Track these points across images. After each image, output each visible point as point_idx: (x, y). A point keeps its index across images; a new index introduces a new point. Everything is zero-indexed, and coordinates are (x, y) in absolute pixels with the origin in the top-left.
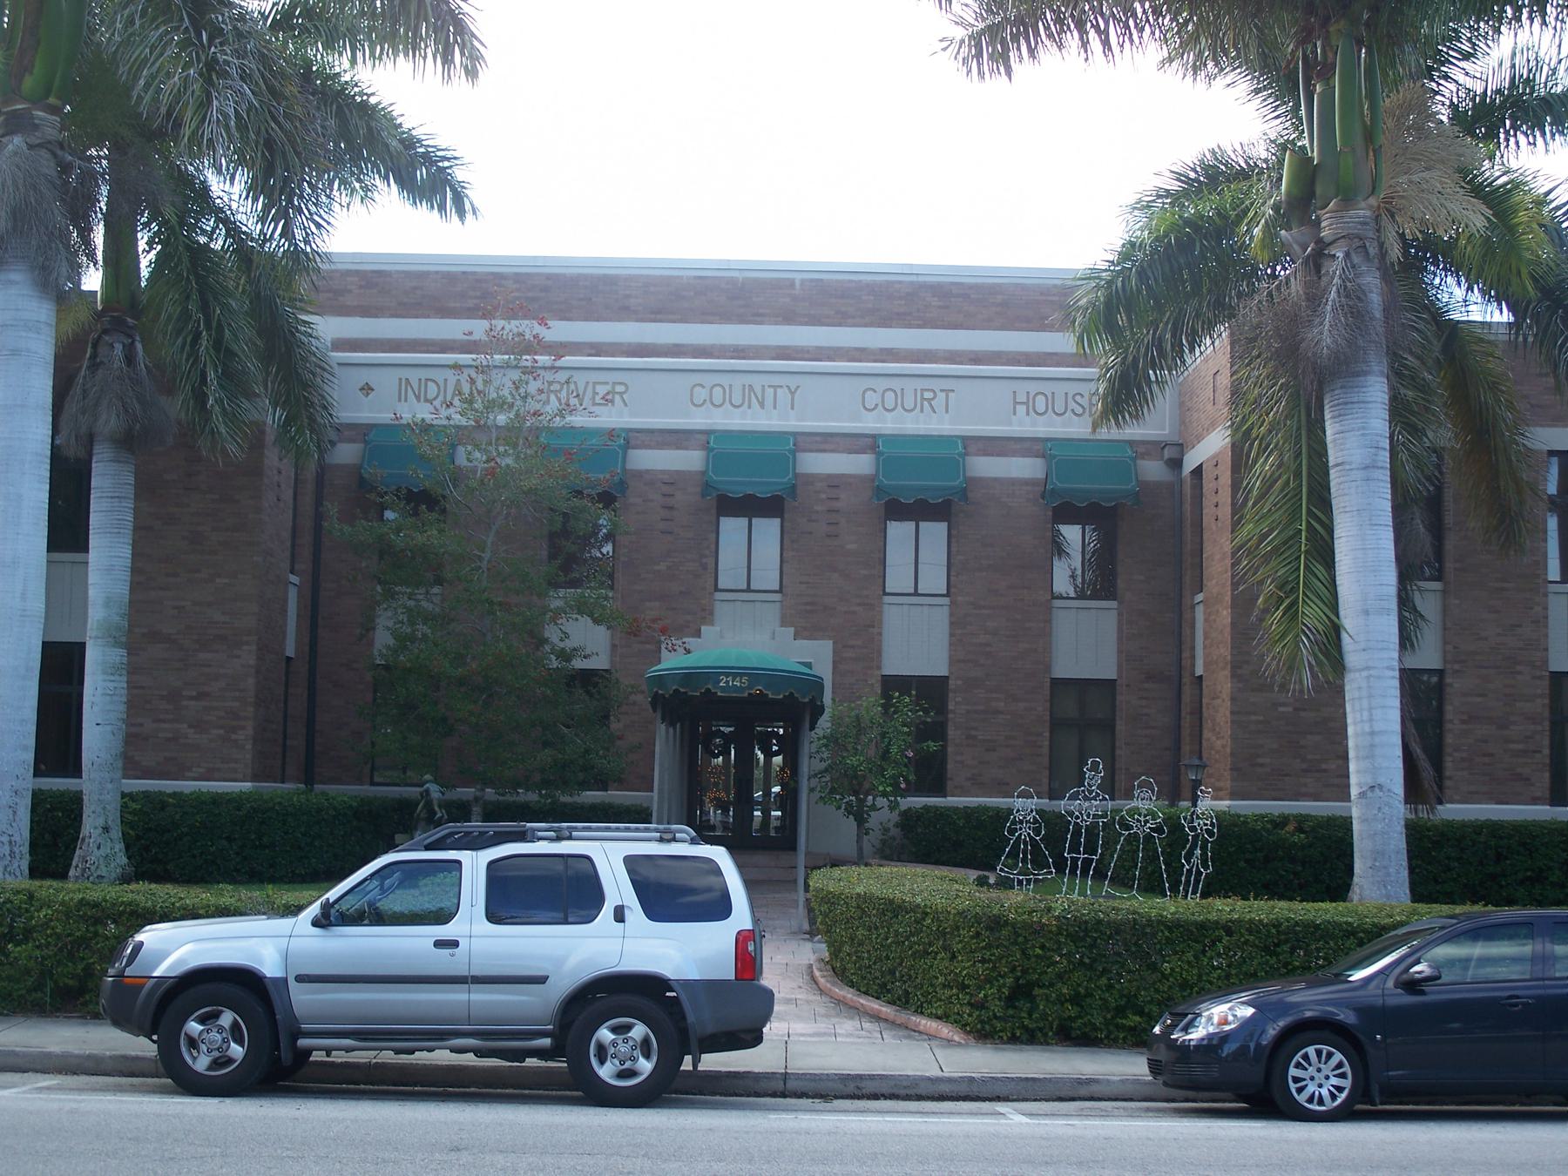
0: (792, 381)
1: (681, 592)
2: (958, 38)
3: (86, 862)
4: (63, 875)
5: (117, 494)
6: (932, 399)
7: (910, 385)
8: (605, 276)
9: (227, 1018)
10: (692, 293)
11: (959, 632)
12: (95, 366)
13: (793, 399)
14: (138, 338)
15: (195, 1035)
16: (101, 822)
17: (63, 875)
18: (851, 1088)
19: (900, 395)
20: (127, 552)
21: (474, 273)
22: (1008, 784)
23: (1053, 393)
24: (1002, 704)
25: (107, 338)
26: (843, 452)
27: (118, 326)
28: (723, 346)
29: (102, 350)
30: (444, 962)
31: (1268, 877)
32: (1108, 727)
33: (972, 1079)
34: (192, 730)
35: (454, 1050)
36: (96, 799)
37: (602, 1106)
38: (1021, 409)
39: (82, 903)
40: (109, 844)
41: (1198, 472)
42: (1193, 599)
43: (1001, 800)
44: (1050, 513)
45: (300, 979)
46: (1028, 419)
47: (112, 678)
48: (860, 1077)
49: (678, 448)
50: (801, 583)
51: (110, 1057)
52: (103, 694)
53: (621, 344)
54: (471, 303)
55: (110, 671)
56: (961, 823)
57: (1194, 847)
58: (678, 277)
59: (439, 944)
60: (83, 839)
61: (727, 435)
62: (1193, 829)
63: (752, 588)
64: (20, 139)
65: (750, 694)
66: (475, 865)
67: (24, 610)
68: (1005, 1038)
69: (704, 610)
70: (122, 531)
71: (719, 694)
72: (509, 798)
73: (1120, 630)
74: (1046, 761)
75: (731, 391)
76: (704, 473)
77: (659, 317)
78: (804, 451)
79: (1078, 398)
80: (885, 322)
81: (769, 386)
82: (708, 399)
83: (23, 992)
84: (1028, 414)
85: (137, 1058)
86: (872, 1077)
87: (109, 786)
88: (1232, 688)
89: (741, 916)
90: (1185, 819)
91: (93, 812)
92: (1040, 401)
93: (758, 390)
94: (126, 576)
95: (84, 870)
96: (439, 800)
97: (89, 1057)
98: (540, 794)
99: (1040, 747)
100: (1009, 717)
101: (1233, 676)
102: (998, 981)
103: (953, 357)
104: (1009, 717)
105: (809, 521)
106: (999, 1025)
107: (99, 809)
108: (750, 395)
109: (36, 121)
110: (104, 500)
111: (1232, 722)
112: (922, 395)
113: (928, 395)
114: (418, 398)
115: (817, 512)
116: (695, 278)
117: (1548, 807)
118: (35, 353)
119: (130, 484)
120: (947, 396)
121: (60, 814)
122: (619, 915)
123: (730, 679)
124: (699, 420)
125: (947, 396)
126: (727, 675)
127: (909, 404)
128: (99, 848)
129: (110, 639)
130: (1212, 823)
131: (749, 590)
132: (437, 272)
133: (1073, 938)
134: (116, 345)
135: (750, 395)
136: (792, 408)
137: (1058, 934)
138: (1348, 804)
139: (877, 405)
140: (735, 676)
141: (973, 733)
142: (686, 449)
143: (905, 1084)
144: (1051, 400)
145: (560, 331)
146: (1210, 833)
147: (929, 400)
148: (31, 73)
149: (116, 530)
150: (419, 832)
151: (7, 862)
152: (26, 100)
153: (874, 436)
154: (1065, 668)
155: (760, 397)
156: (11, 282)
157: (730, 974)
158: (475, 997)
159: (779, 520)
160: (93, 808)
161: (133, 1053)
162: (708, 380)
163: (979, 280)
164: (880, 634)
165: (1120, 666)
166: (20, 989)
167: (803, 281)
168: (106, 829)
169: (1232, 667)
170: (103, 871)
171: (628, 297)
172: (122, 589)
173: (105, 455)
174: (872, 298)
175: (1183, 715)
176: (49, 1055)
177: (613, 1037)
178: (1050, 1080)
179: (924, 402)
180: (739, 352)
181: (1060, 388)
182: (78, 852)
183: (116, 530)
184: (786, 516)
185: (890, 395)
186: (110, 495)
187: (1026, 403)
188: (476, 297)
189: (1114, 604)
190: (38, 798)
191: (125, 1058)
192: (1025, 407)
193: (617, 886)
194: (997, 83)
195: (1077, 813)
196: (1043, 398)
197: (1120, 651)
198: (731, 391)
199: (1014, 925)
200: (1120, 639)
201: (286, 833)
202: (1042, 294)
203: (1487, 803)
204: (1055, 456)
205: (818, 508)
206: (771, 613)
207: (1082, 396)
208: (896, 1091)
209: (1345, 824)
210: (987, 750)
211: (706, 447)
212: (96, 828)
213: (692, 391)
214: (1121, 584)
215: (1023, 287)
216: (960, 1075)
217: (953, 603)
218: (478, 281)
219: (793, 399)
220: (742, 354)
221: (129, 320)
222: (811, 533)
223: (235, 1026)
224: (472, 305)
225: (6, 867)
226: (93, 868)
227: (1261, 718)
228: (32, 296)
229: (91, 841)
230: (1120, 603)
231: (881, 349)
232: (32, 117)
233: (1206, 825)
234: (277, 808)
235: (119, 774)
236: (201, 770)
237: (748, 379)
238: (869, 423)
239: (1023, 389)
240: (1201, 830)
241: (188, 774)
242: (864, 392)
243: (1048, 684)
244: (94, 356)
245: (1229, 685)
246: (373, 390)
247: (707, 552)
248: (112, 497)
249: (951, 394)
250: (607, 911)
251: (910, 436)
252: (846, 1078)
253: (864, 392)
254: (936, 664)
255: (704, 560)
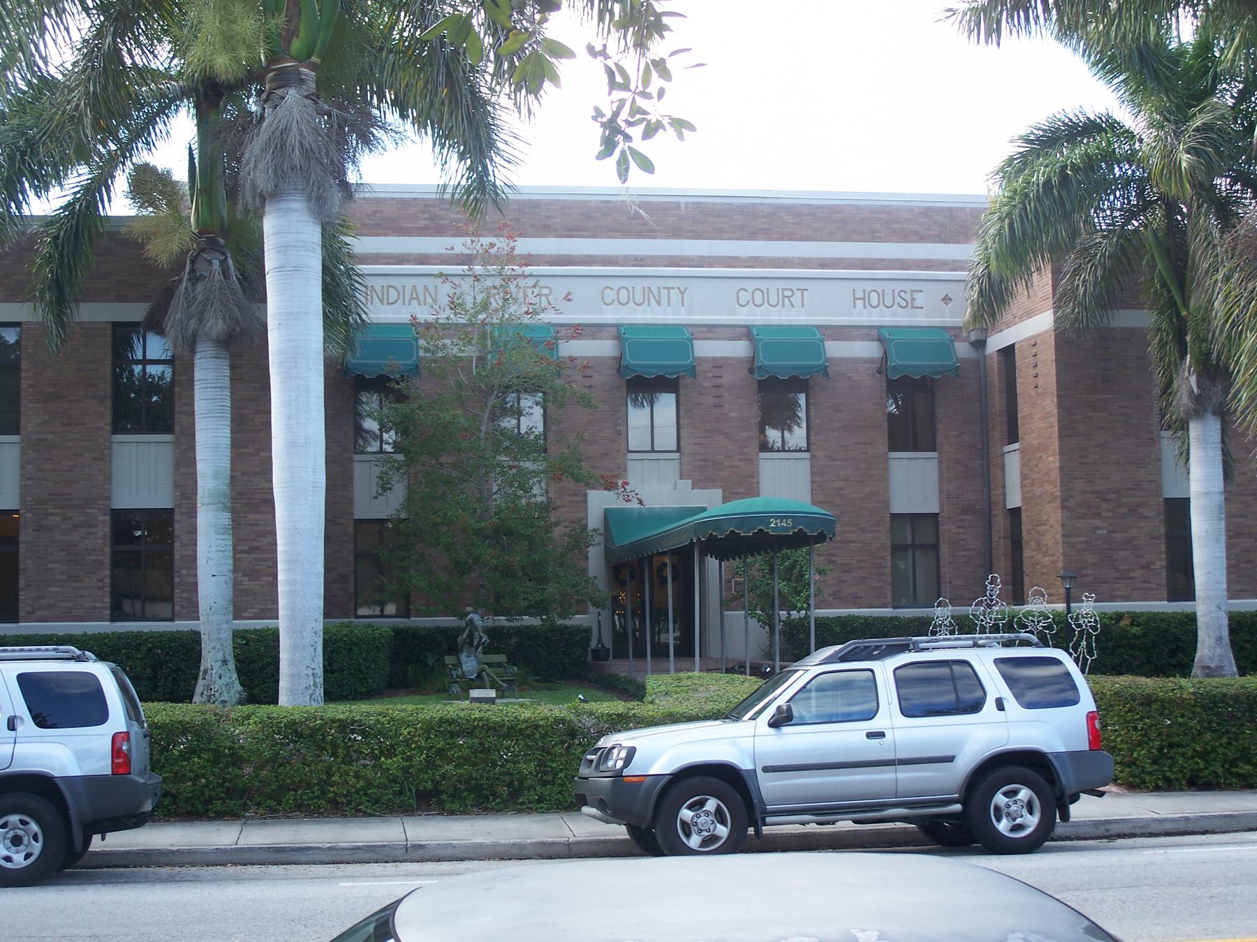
0: (682, 284)
1: (601, 454)
2: (961, 11)
3: (211, 689)
4: (188, 698)
5: (219, 385)
6: (791, 296)
7: (773, 286)
8: (529, 201)
9: (711, 804)
10: (599, 215)
11: (819, 479)
12: (195, 279)
13: (683, 298)
14: (229, 255)
15: (688, 820)
16: (220, 656)
17: (188, 698)
18: (1101, 831)
19: (766, 294)
20: (228, 433)
21: (423, 199)
22: (861, 597)
23: (883, 291)
24: (854, 535)
25: (205, 255)
26: (723, 340)
27: (212, 244)
28: (626, 257)
29: (201, 267)
30: (876, 750)
31: (1116, 661)
32: (934, 548)
33: (1187, 819)
34: (246, 578)
35: (855, 822)
36: (215, 637)
37: (31, 886)
38: (859, 303)
39: (442, 721)
40: (228, 675)
41: (1008, 352)
42: (1002, 449)
43: (856, 610)
44: (885, 384)
45: (766, 769)
46: (865, 311)
47: (223, 537)
48: (1108, 822)
49: (593, 339)
50: (695, 444)
51: (531, 844)
52: (217, 551)
53: (544, 256)
54: (421, 224)
55: (221, 531)
56: (838, 629)
57: (1080, 638)
58: (587, 201)
59: (870, 735)
60: (205, 672)
61: (633, 327)
62: (1079, 626)
63: (656, 449)
64: (295, 91)
65: (794, 532)
66: (884, 670)
67: (316, 482)
68: (1151, 787)
69: (619, 468)
70: (224, 415)
71: (771, 533)
72: (516, 624)
73: (940, 473)
74: (889, 579)
75: (633, 291)
76: (619, 359)
77: (573, 233)
78: (698, 339)
79: (902, 294)
80: (752, 236)
81: (664, 288)
82: (616, 299)
83: (391, 796)
84: (865, 307)
85: (553, 843)
86: (1117, 821)
87: (225, 626)
88: (1062, 517)
89: (117, 719)
90: (1071, 618)
91: (214, 648)
92: (874, 296)
93: (655, 291)
94: (227, 452)
95: (209, 697)
96: (482, 627)
97: (514, 845)
98: (542, 619)
99: (885, 567)
100: (859, 545)
101: (1063, 508)
102: (1147, 744)
103: (805, 263)
104: (859, 545)
105: (700, 395)
106: (1147, 778)
107: (218, 646)
108: (649, 296)
109: (303, 77)
110: (209, 390)
111: (1063, 543)
112: (783, 294)
113: (788, 293)
114: (381, 301)
115: (705, 387)
116: (602, 202)
117: (1166, 602)
118: (313, 269)
119: (226, 376)
120: (802, 294)
121: (160, 652)
122: (1000, 705)
123: (778, 521)
124: (610, 315)
125: (802, 294)
126: (776, 518)
127: (773, 300)
128: (220, 678)
129: (221, 505)
130: (1096, 621)
131: (653, 451)
132: (393, 199)
133: (1204, 707)
134: (213, 261)
135: (649, 296)
136: (683, 305)
137: (1194, 706)
138: (1193, 603)
139: (748, 302)
140: (782, 518)
141: (833, 558)
142: (600, 339)
143: (1140, 825)
144: (881, 295)
145: (524, 246)
146: (1095, 629)
147: (789, 297)
148: (298, 36)
149: (220, 415)
150: (464, 654)
151: (311, 691)
152: (295, 59)
153: (747, 327)
154: (901, 505)
155: (427, 294)
156: (290, 210)
157: (1086, 747)
158: (900, 775)
159: (674, 395)
160: (212, 645)
161: (549, 840)
162: (617, 283)
163: (823, 202)
164: (758, 483)
165: (941, 502)
166: (387, 794)
167: (687, 204)
168: (225, 662)
169: (1062, 500)
170: (226, 697)
171: (549, 217)
172: (225, 463)
173: (208, 353)
174: (741, 217)
175: (995, 538)
176: (480, 846)
177: (1007, 800)
178: (1242, 816)
179: (785, 299)
180: (639, 261)
181: (889, 287)
182: (200, 682)
183: (220, 415)
184: (681, 391)
185: (758, 294)
186: (214, 385)
187: (863, 299)
188: (426, 219)
189: (934, 454)
190: (237, 634)
191: (598, 842)
192: (862, 301)
193: (994, 684)
194: (987, 51)
195: (982, 617)
196: (876, 294)
197: (941, 492)
198: (633, 291)
199: (1163, 701)
200: (941, 482)
201: (351, 659)
202: (872, 213)
203: (1251, 599)
204: (628, 339)
205: (706, 384)
206: (671, 468)
207: (905, 292)
208: (1134, 831)
209: (1192, 619)
210: (844, 572)
211: (619, 338)
212: (216, 661)
213: (738, 294)
214: (940, 439)
215: (857, 208)
216: (1179, 815)
217: (813, 457)
218: (427, 206)
219: (683, 298)
220: (641, 263)
221: (221, 240)
222: (701, 404)
223: (719, 811)
224: (422, 226)
225: (311, 695)
226: (217, 695)
227: (1084, 539)
228: (308, 222)
229: (214, 672)
230: (940, 453)
231: (750, 258)
232: (299, 73)
233: (1090, 622)
234: (345, 639)
235: (231, 617)
236: (256, 611)
237: (646, 283)
238: (744, 316)
239: (860, 287)
240: (1086, 626)
241: (244, 614)
242: (603, 290)
243: (889, 518)
244: (192, 271)
245: (1060, 515)
246: (951, 300)
247: (620, 421)
248: (215, 387)
249: (805, 292)
250: (990, 704)
251: (775, 326)
252: (1097, 824)
253: (603, 290)
254: (930, 505)
255: (618, 428)
